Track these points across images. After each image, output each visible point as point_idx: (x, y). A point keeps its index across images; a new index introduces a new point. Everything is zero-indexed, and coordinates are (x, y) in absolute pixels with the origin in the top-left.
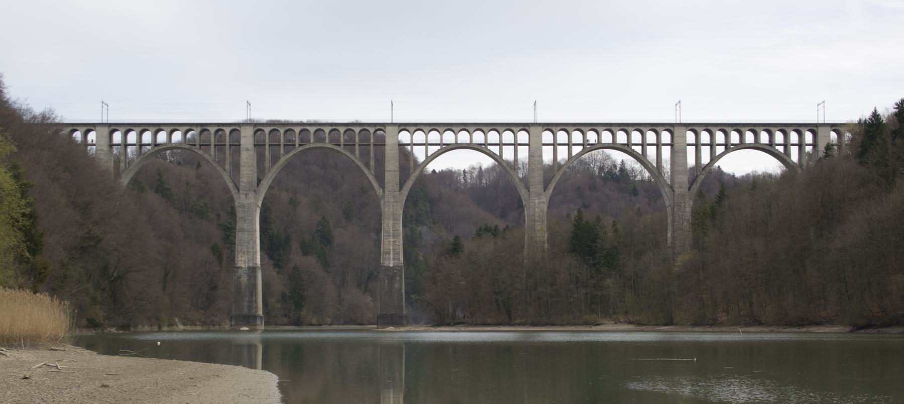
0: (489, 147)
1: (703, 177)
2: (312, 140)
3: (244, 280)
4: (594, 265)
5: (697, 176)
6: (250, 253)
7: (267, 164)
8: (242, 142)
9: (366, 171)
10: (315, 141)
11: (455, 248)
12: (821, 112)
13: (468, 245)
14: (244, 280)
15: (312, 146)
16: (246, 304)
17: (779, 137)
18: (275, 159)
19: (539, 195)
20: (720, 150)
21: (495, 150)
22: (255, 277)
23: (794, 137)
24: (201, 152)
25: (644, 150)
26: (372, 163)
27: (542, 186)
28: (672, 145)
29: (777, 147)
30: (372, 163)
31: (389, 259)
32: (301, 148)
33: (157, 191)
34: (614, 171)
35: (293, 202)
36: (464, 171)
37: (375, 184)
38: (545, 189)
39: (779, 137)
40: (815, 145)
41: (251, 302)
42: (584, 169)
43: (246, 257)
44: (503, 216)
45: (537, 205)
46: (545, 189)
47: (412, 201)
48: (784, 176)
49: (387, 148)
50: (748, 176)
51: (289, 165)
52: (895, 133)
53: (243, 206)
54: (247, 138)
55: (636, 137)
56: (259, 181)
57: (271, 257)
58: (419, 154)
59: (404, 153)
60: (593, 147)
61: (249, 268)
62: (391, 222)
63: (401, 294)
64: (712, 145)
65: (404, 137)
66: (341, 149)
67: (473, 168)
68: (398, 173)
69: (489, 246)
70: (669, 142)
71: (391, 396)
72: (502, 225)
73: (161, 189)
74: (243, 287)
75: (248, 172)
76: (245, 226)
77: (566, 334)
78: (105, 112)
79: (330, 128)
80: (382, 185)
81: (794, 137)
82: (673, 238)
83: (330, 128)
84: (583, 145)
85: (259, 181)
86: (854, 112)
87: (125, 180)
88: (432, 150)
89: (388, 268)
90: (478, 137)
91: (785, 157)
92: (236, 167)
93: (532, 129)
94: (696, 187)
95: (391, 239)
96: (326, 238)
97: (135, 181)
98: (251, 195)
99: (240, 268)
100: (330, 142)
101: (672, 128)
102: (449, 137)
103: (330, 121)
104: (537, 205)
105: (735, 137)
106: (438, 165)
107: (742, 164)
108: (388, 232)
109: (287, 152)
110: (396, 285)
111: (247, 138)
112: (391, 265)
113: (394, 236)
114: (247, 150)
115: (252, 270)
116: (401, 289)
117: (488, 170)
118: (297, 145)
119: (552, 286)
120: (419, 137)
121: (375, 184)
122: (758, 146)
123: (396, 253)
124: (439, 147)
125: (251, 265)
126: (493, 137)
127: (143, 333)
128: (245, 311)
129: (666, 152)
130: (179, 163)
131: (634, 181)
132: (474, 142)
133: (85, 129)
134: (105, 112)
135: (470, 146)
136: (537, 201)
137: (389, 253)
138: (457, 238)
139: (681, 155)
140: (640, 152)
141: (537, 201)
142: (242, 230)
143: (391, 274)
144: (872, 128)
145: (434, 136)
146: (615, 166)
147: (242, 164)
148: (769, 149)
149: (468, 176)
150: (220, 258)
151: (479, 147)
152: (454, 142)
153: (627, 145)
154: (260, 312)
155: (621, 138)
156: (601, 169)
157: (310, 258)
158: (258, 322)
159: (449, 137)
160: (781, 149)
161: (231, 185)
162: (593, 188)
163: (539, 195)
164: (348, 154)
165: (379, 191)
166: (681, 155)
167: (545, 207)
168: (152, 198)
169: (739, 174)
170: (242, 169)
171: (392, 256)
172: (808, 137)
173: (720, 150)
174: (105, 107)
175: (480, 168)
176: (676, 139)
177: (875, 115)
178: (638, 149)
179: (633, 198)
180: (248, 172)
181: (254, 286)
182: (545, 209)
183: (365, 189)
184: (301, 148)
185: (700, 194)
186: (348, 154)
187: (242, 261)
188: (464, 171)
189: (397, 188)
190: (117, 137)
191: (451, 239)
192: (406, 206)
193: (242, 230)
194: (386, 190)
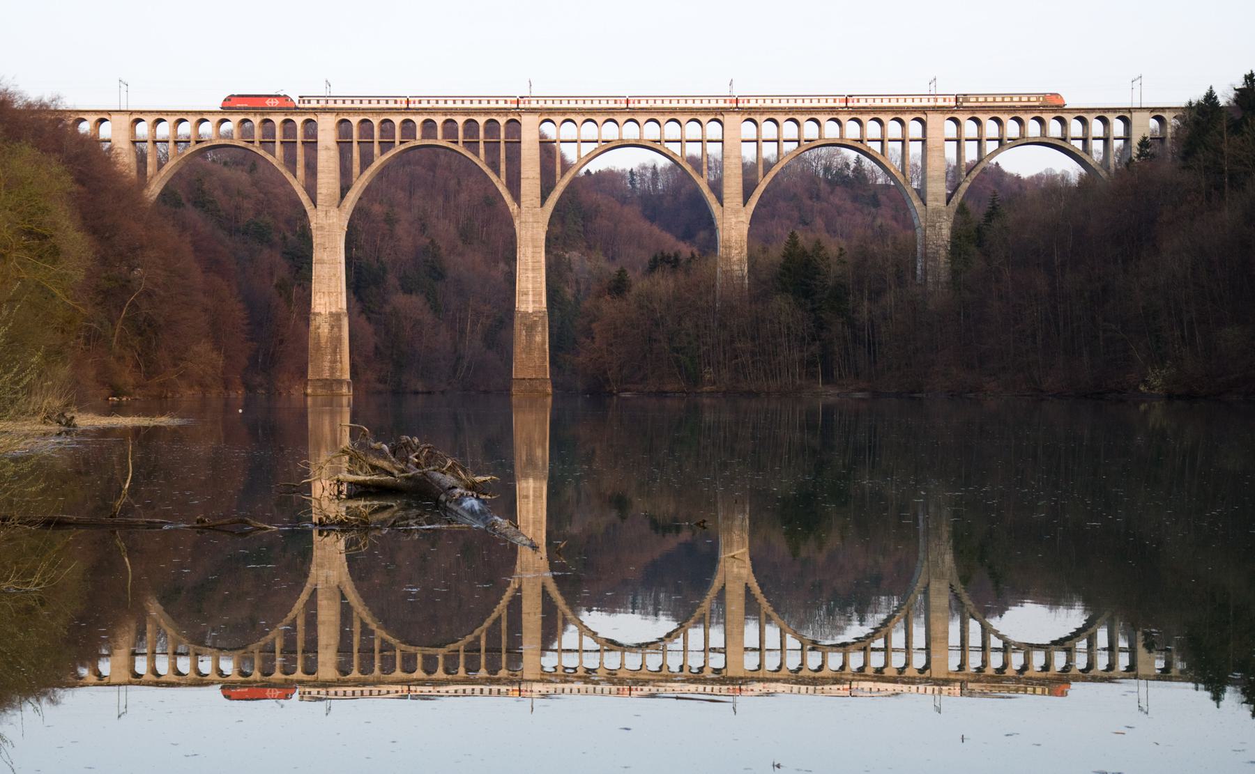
0: (667, 145)
1: (967, 185)
2: (419, 135)
3: (325, 330)
4: (813, 310)
5: (959, 185)
6: (329, 294)
7: (356, 168)
8: (320, 138)
10: (423, 137)
11: (619, 286)
12: (1137, 91)
13: (640, 283)
14: (325, 330)
15: (418, 143)
16: (327, 364)
18: (366, 161)
19: (737, 212)
20: (991, 147)
24: (261, 152)
26: (503, 167)
27: (741, 200)
28: (924, 141)
29: (1073, 142)
30: (503, 167)
31: (527, 302)
34: (846, 173)
35: (390, 220)
36: (631, 172)
39: (1076, 128)
40: (1127, 139)
42: (803, 170)
43: (327, 299)
44: (687, 236)
45: (734, 224)
47: (558, 217)
48: (1083, 181)
49: (523, 146)
50: (1039, 177)
51: (385, 169)
52: (1236, 128)
53: (322, 228)
54: (327, 130)
55: (873, 130)
56: (343, 196)
57: (360, 299)
58: (570, 153)
59: (547, 147)
60: (813, 144)
61: (331, 314)
62: (530, 250)
64: (1106, 140)
65: (549, 130)
66: (460, 148)
67: (645, 168)
68: (539, 182)
69: (664, 284)
70: (920, 136)
72: (685, 249)
73: (201, 201)
74: (323, 341)
75: (328, 180)
78: (124, 94)
80: (517, 197)
81: (1097, 128)
82: (925, 272)
84: (799, 141)
85: (343, 196)
86: (1180, 90)
87: (154, 190)
88: (587, 148)
89: (526, 314)
91: (1084, 156)
92: (311, 169)
93: (727, 119)
94: (957, 199)
95: (530, 275)
96: (437, 273)
97: (167, 195)
98: (334, 212)
99: (319, 314)
100: (444, 137)
102: (610, 131)
104: (734, 224)
105: (1012, 129)
106: (595, 167)
107: (1026, 163)
108: (526, 264)
109: (382, 153)
112: (530, 311)
114: (327, 148)
115: (336, 317)
116: (544, 343)
117: (663, 169)
118: (397, 143)
119: (753, 339)
120: (568, 131)
121: (304, 198)
122: (1046, 140)
124: (596, 145)
125: (334, 310)
127: (365, 506)
128: (326, 375)
129: (915, 149)
130: (225, 164)
131: (874, 185)
132: (645, 137)
133: (96, 117)
134: (124, 94)
135: (612, 645)
136: (734, 220)
137: (526, 294)
138: (622, 272)
139: (936, 154)
141: (734, 220)
142: (322, 262)
144: (1204, 113)
145: (589, 131)
146: (847, 165)
147: (319, 168)
148: (1060, 146)
149: (637, 178)
152: (617, 138)
154: (347, 376)
155: (852, 131)
156: (827, 169)
157: (414, 298)
159: (610, 131)
160: (1078, 145)
161: (304, 198)
162: (815, 196)
163: (737, 212)
164: (469, 155)
165: (513, 207)
166: (936, 154)
167: (745, 228)
168: (193, 214)
169: (1025, 174)
170: (319, 175)
171: (531, 298)
172: (1118, 128)
173: (991, 147)
174: (124, 87)
175: (654, 167)
176: (929, 132)
177: (1210, 97)
178: (876, 147)
179: (873, 210)
180: (328, 180)
181: (339, 339)
182: (746, 232)
183: (492, 201)
184: (403, 147)
185: (962, 210)
186: (469, 155)
188: (631, 172)
189: (538, 202)
190: (143, 130)
191: (614, 269)
192: (551, 223)
193: (322, 262)
194: (523, 205)
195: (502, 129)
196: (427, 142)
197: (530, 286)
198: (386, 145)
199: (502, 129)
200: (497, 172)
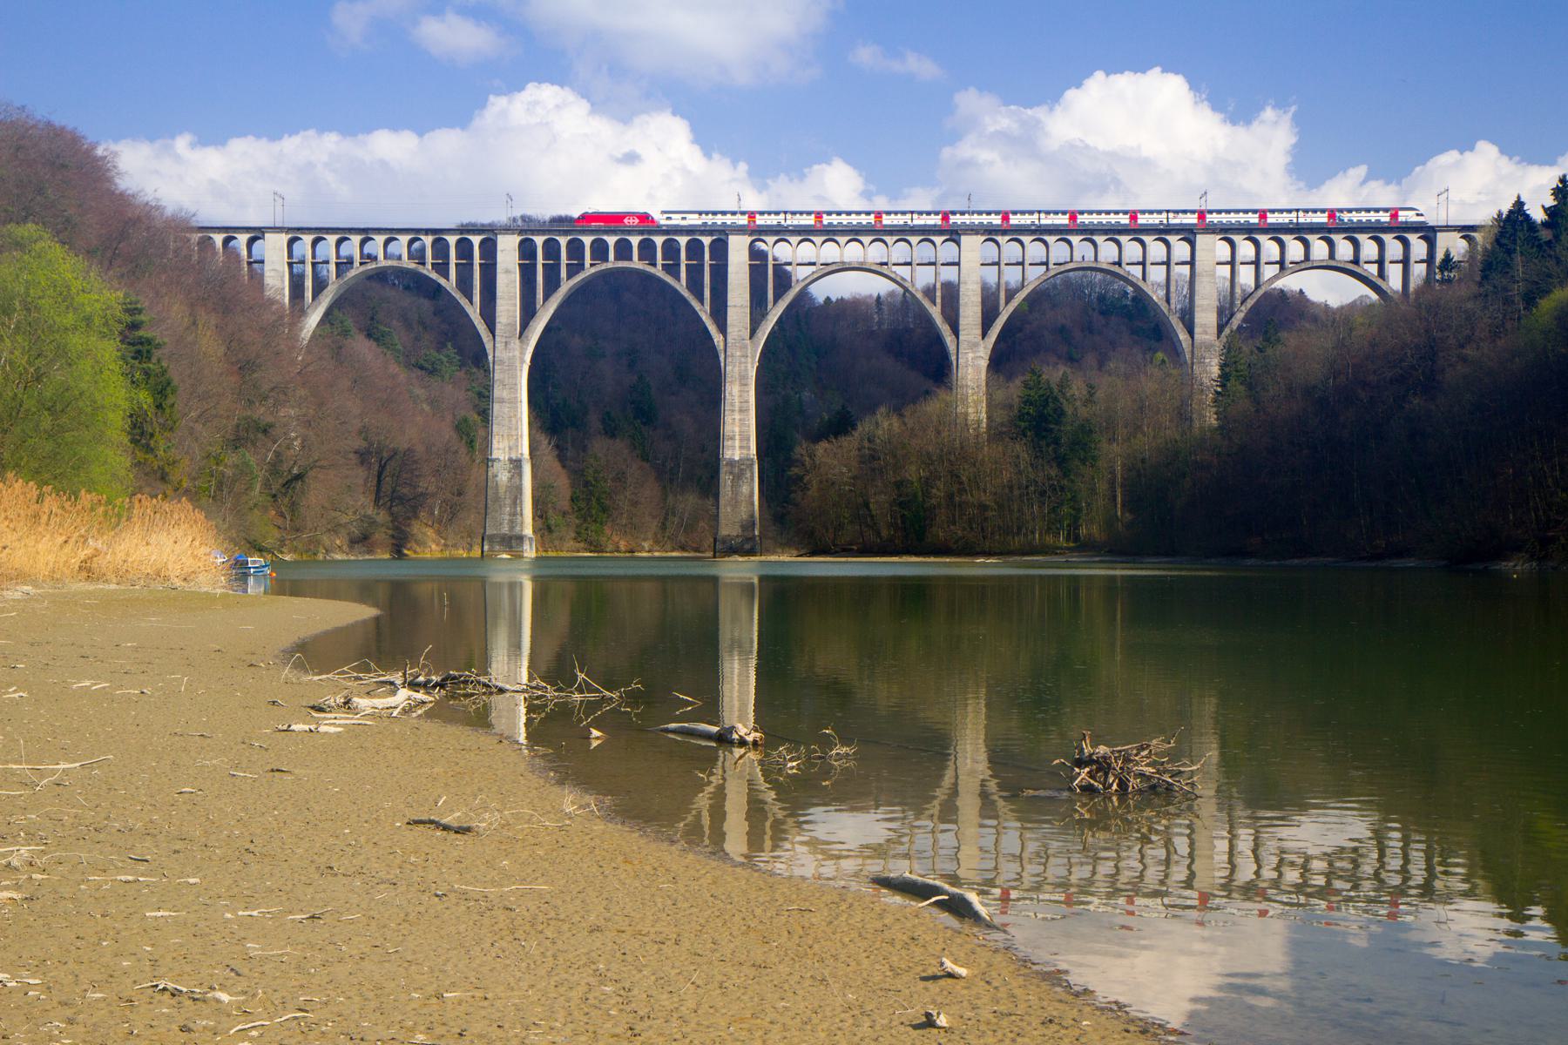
3: (503, 476)
9: (463, 302)
17: (1369, 249)
18: (552, 284)
21: (904, 272)
22: (520, 475)
23: (1394, 248)
25: (1382, 273)
27: (979, 332)
29: (1366, 266)
31: (733, 447)
32: (362, 269)
33: (369, 336)
37: (945, 330)
38: (984, 335)
39: (1369, 249)
41: (515, 514)
46: (984, 335)
49: (267, 267)
58: (801, 273)
63: (752, 504)
71: (736, 665)
76: (505, 394)
77: (672, 564)
79: (408, 237)
80: (723, 329)
81: (1394, 248)
83: (408, 237)
89: (731, 463)
90: (875, 252)
91: (1379, 282)
95: (737, 416)
101: (1431, 234)
103: (362, 226)
107: (1330, 291)
108: (732, 404)
110: (745, 489)
111: (508, 249)
113: (741, 411)
114: (507, 271)
121: (945, 330)
122: (1333, 263)
123: (745, 438)
124: (813, 268)
126: (899, 251)
128: (505, 529)
137: (732, 438)
140: (1140, 276)
143: (739, 468)
148: (1352, 270)
150: (471, 443)
151: (878, 268)
153: (1119, 264)
154: (528, 531)
158: (526, 546)
160: (1373, 269)
163: (974, 346)
167: (984, 363)
171: (737, 443)
172: (1419, 248)
181: (519, 489)
184: (593, 270)
187: (500, 450)
193: (502, 401)
195: (707, 250)
196: (621, 264)
197: (737, 429)
198: (573, 270)
199: (707, 250)
200: (701, 301)
